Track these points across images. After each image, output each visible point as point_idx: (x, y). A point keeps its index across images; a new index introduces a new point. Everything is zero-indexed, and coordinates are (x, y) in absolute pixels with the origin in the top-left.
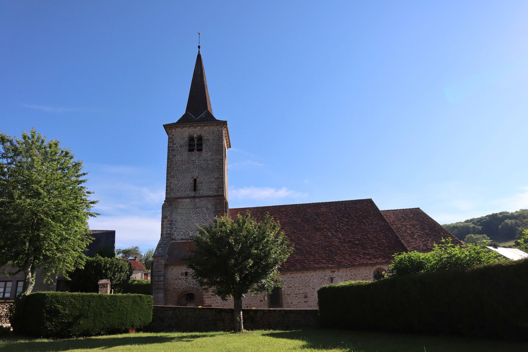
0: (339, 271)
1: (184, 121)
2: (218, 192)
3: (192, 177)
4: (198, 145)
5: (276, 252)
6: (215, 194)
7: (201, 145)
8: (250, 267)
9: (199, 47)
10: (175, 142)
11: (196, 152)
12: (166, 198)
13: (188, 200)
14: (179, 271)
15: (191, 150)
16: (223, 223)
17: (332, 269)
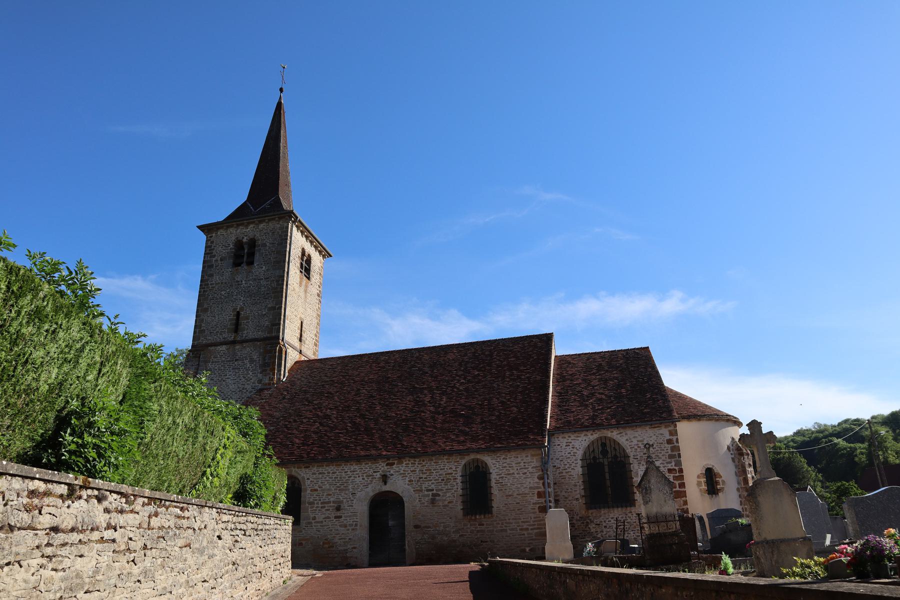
0: (400, 463)
1: (239, 216)
3: (234, 310)
9: (281, 90)
13: (224, 348)
15: (237, 264)
17: (388, 459)
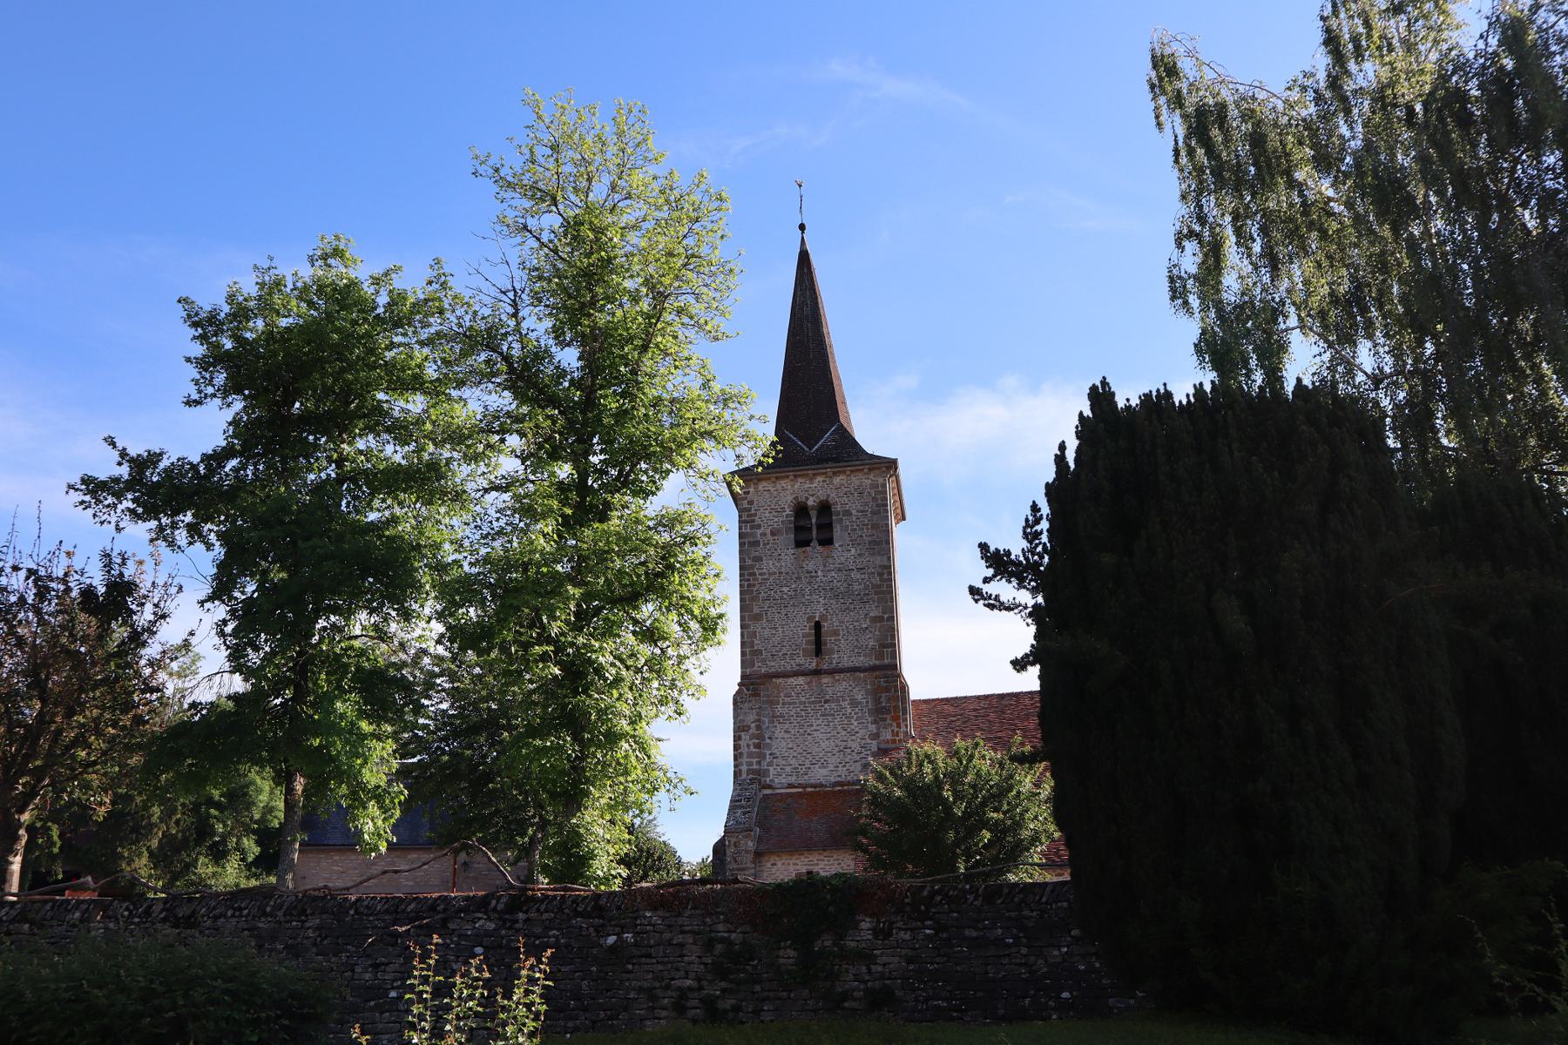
2: (880, 656)
3: (810, 619)
4: (819, 527)
5: (1036, 818)
6: (874, 662)
7: (830, 526)
8: (985, 847)
9: (802, 227)
10: (758, 521)
11: (816, 549)
12: (743, 677)
13: (801, 680)
14: (791, 868)
15: (801, 543)
16: (927, 756)
